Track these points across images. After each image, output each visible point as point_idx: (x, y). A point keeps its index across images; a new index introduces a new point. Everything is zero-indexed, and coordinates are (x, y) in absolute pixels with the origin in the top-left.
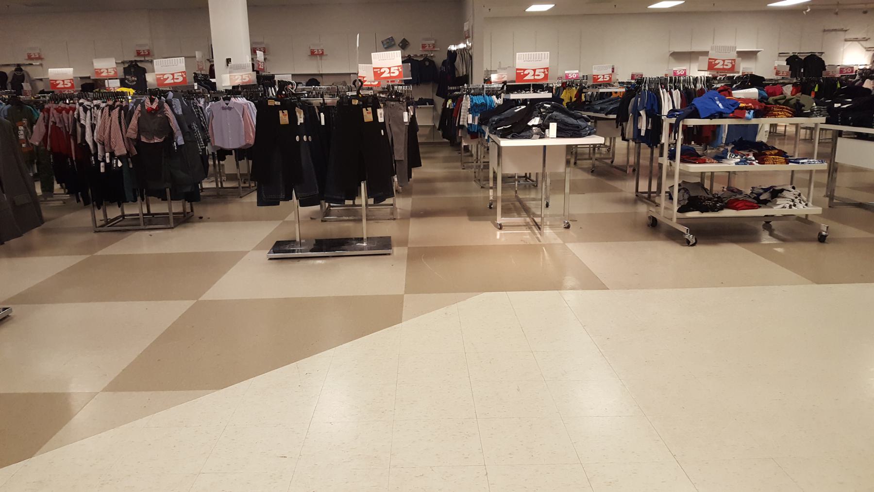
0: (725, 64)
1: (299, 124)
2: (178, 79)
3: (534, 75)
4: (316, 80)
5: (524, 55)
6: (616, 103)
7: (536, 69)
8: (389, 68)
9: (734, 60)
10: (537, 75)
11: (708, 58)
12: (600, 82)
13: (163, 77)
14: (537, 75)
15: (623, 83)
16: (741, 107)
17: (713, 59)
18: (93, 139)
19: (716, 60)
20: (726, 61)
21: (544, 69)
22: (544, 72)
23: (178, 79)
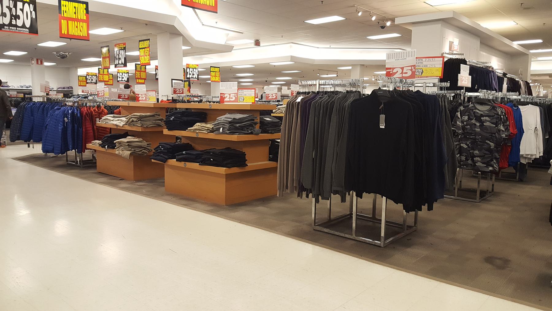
0: (231, 97)
1: (426, 204)
4: (480, 25)
5: (229, 84)
6: (190, 130)
7: (403, 68)
9: (277, 93)
10: (405, 73)
11: (291, 90)
12: (270, 99)
13: (393, 71)
14: (405, 73)
15: (178, 102)
16: (86, 18)
17: (267, 94)
18: (30, 11)
19: (269, 94)
20: (273, 95)
21: (411, 66)
22: (411, 70)
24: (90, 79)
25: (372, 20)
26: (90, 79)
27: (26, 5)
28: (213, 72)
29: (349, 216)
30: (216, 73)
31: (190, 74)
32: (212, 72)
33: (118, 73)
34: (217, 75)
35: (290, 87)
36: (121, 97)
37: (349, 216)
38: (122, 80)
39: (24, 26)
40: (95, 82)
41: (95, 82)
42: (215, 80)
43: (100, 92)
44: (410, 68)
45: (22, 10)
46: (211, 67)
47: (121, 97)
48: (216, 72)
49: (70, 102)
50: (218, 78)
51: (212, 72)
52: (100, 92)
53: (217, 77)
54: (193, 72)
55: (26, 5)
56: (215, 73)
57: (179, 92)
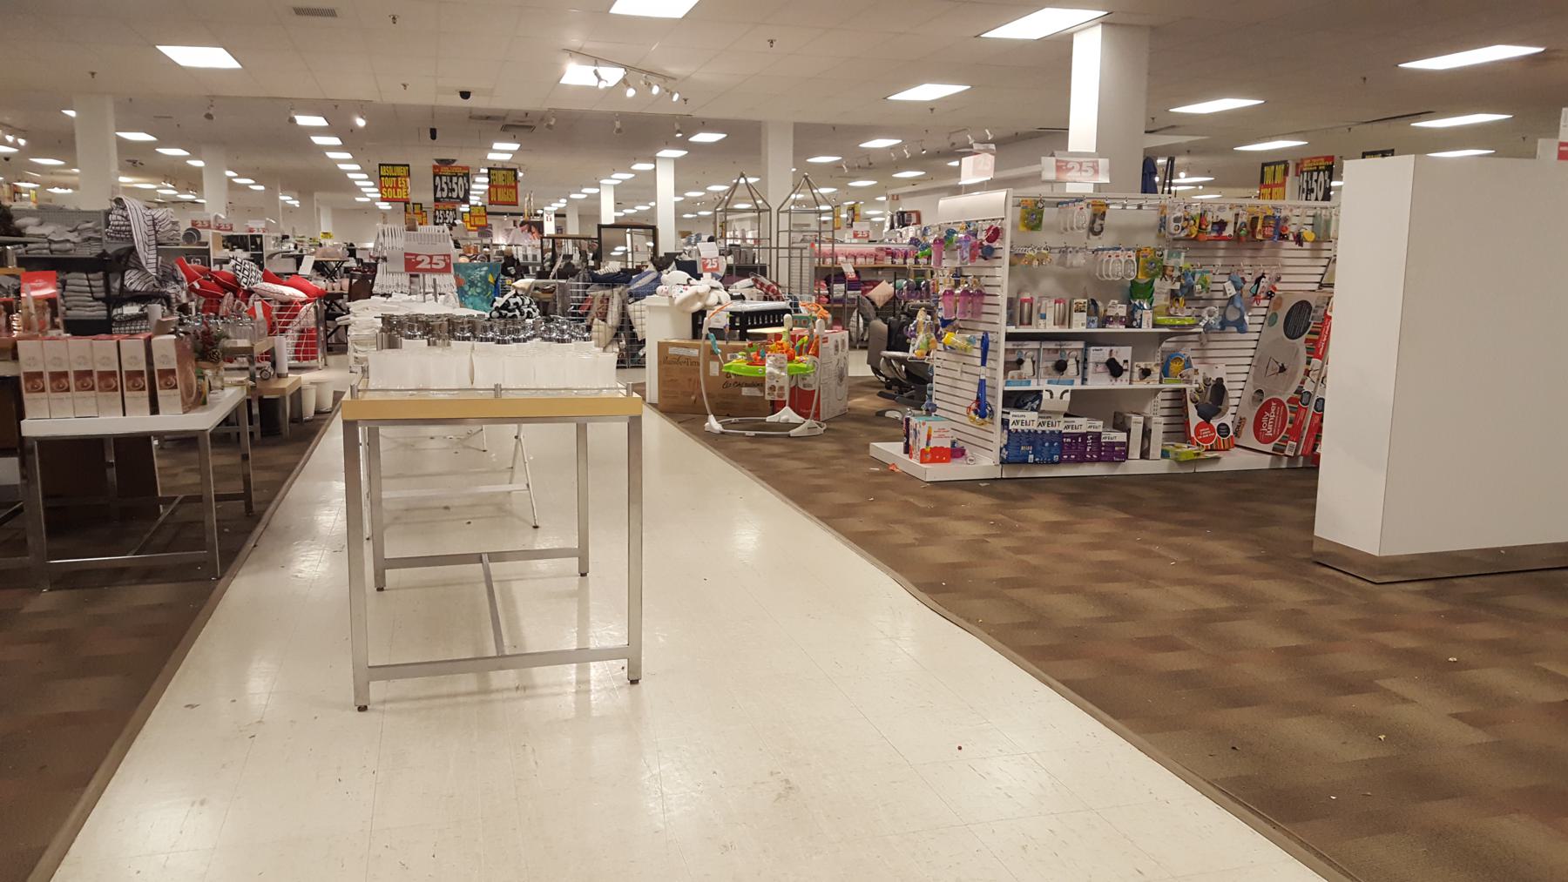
2: (437, 264)
3: (431, 263)
8: (431, 257)
10: (435, 264)
14: (435, 264)
21: (444, 255)
23: (437, 264)
24: (444, 186)
25: (366, 126)
26: (444, 186)
27: (461, 178)
28: (389, 177)
29: (1320, 353)
30: (399, 179)
31: (442, 190)
32: (385, 177)
33: (438, 178)
34: (402, 184)
35: (1219, 407)
36: (420, 266)
37: (1320, 353)
38: (450, 195)
39: (458, 197)
40: (461, 196)
41: (461, 196)
42: (395, 197)
43: (708, 261)
44: (442, 258)
45: (457, 184)
46: (380, 165)
47: (420, 266)
48: (397, 177)
49: (122, 238)
50: (404, 190)
51: (385, 177)
52: (708, 261)
53: (401, 188)
54: (450, 184)
55: (461, 178)
56: (394, 179)
57: (429, 267)
